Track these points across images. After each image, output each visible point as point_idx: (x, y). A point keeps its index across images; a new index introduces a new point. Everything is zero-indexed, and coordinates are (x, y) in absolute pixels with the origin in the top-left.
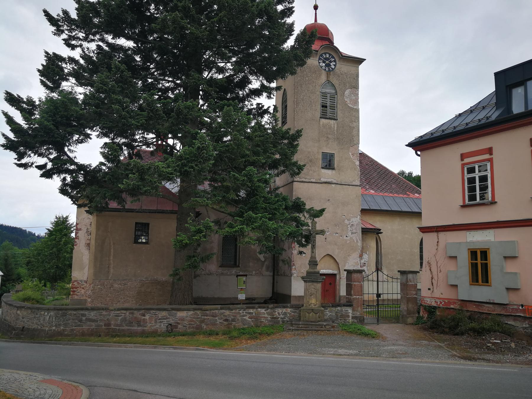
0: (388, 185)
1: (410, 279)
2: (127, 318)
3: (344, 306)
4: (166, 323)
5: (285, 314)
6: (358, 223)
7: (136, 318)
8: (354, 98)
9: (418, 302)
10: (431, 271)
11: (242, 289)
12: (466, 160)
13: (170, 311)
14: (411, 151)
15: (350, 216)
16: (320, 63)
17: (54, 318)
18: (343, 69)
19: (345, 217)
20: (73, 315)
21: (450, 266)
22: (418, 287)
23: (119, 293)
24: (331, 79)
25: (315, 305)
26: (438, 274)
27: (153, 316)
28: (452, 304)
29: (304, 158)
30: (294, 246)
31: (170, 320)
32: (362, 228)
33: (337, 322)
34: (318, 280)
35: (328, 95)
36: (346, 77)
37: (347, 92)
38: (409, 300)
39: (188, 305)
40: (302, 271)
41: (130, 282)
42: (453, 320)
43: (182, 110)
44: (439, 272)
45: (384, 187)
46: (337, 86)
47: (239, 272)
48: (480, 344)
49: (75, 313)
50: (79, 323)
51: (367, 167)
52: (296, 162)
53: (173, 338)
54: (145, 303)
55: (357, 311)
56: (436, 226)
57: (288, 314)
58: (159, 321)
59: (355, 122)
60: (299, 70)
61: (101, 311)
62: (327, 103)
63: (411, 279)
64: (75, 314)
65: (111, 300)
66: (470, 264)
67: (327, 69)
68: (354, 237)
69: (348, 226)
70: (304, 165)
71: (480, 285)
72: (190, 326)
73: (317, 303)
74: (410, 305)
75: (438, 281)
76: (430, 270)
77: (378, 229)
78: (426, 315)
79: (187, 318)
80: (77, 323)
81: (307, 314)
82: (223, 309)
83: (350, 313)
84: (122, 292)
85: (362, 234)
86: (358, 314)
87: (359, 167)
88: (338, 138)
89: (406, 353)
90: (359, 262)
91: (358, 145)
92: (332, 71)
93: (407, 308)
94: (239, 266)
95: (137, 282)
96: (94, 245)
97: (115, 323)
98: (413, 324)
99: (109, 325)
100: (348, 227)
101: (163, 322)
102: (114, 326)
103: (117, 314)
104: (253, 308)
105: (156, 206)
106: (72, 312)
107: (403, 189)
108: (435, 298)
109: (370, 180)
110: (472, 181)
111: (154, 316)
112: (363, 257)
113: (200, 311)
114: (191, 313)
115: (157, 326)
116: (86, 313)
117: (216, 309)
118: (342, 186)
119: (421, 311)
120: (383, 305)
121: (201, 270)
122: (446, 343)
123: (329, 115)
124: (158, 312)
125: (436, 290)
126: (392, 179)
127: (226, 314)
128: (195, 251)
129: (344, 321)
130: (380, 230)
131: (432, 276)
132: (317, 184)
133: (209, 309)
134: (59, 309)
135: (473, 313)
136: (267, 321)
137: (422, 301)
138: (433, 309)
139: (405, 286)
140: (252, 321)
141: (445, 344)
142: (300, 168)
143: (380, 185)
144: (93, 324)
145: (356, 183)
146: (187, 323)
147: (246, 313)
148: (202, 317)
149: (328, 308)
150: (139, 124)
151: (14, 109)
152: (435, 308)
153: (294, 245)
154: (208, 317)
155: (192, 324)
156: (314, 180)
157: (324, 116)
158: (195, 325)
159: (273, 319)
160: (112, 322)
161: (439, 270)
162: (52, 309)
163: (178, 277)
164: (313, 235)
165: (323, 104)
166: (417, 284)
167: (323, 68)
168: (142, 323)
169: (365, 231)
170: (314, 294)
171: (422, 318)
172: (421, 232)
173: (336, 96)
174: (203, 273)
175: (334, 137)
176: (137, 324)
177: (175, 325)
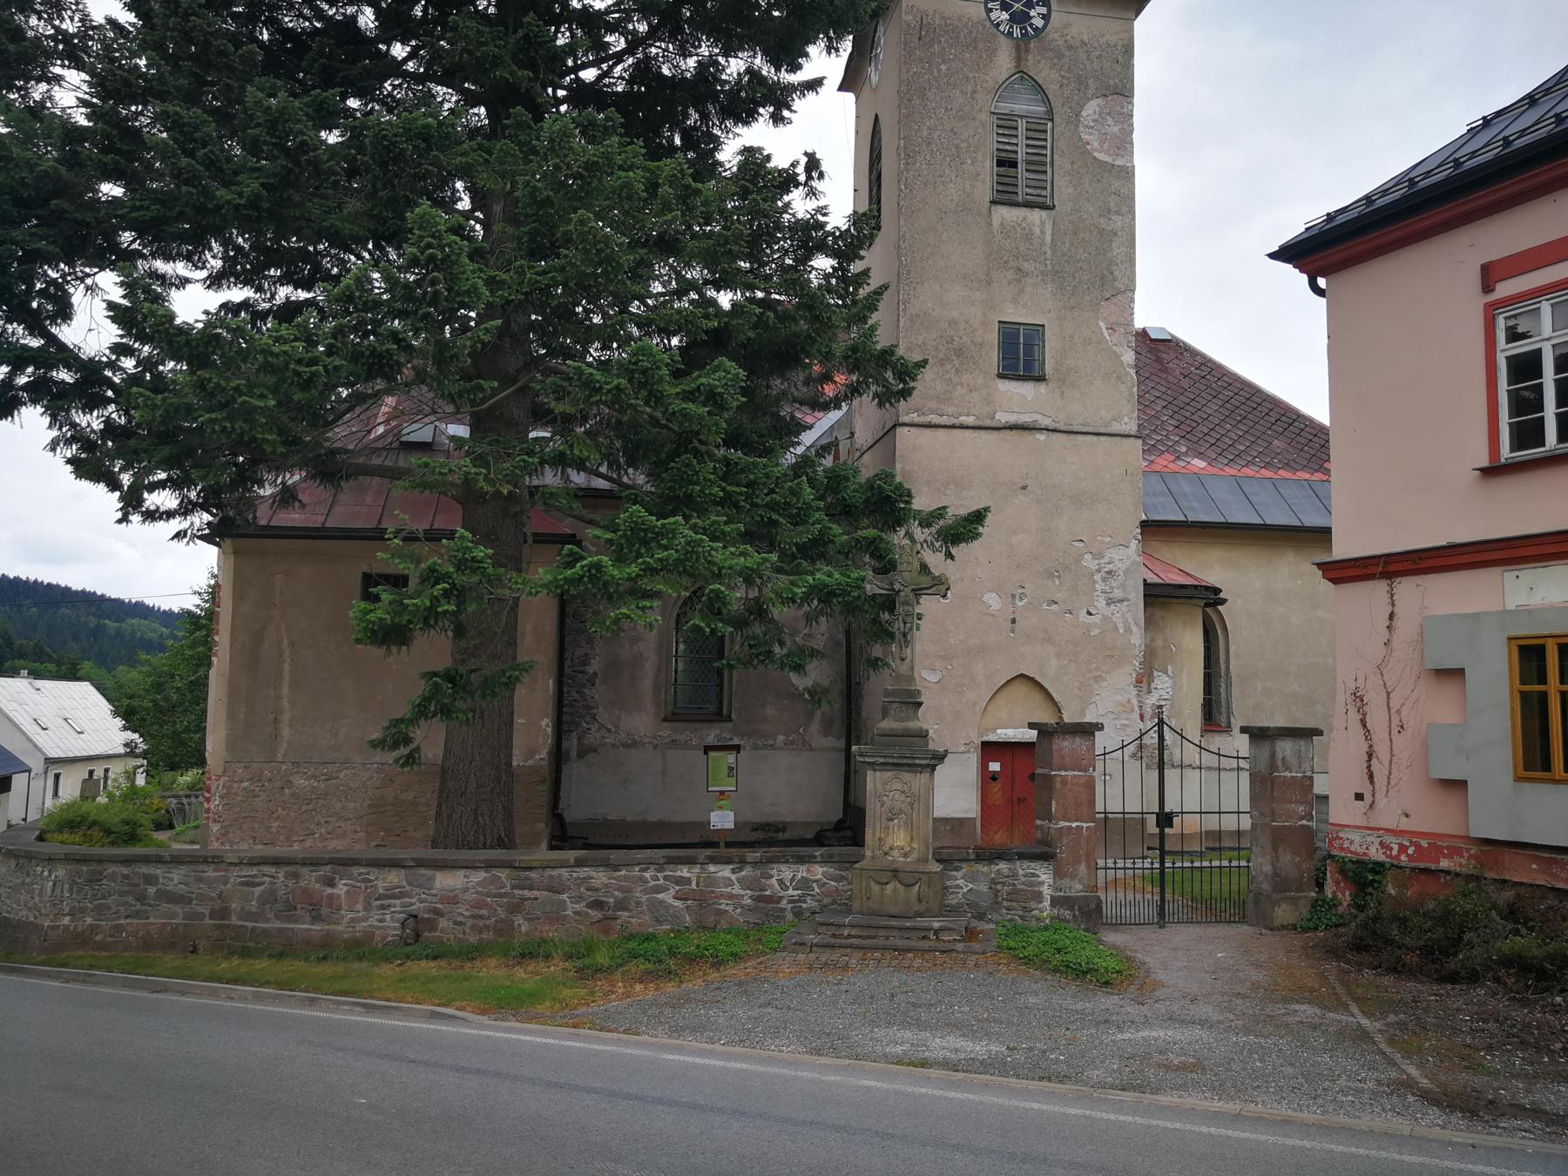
0: (1259, 441)
1: (1284, 758)
2: (281, 893)
3: (1022, 856)
4: (400, 913)
5: (805, 884)
7: (305, 891)
8: (1115, 129)
9: (1320, 844)
10: (1365, 726)
11: (722, 793)
12: (1504, 289)
13: (412, 871)
14: (1293, 278)
15: (1103, 542)
16: (991, 10)
17: (66, 886)
18: (1073, 31)
19: (1082, 544)
20: (119, 878)
21: (1440, 708)
22: (1318, 789)
23: (310, 807)
24: (1032, 64)
25: (906, 855)
26: (1391, 740)
27: (358, 884)
28: (1445, 857)
29: (934, 343)
31: (414, 900)
33: (996, 917)
34: (918, 762)
35: (1022, 125)
36: (1084, 56)
37: (1091, 109)
38: (1278, 838)
39: (492, 847)
41: (346, 768)
42: (1444, 918)
43: (393, 143)
44: (1395, 732)
45: (1242, 448)
46: (1051, 89)
47: (731, 739)
48: (1538, 1028)
49: (125, 871)
50: (139, 907)
51: (1185, 383)
52: (889, 352)
53: (401, 965)
54: (397, 838)
55: (1073, 877)
56: (1381, 556)
57: (815, 885)
58: (379, 903)
59: (1117, 213)
60: (916, 40)
61: (201, 867)
62: (1016, 152)
63: (1288, 759)
64: (126, 877)
65: (284, 827)
66: (1518, 696)
67: (1017, 32)
68: (1118, 614)
69: (1095, 577)
70: (924, 363)
71: (1559, 782)
72: (477, 922)
73: (915, 846)
74: (1287, 859)
75: (1390, 764)
76: (1363, 723)
77: (1207, 588)
78: (1347, 893)
79: (467, 896)
80: (132, 905)
81: (876, 888)
82: (586, 866)
83: (1043, 883)
84: (321, 801)
85: (1146, 605)
86: (1076, 888)
87: (1132, 372)
88: (1057, 272)
89: (1198, 1066)
90: (1135, 702)
91: (1129, 294)
92: (1033, 37)
93: (1273, 865)
94: (729, 719)
95: (369, 769)
96: (228, 648)
97: (242, 908)
98: (1295, 929)
99: (223, 913)
100: (1095, 582)
101: (389, 906)
102: (240, 919)
103: (249, 876)
104: (690, 861)
105: (431, 518)
106: (117, 870)
107: (1313, 452)
108: (1379, 829)
109: (1194, 425)
110: (1525, 367)
111: (363, 885)
112: (1153, 685)
113: (508, 871)
114: (478, 876)
115: (373, 922)
116: (158, 871)
117: (562, 864)
118: (1072, 436)
119: (1329, 880)
120: (1239, 849)
122: (1392, 1018)
123: (1022, 192)
124: (373, 874)
125: (1385, 800)
126: (1273, 420)
127: (595, 883)
128: (582, 668)
129: (1021, 913)
130: (1217, 591)
131: (1371, 746)
132: (982, 433)
133: (538, 864)
134: (77, 858)
135: (1523, 891)
136: (738, 911)
137: (1330, 841)
138: (1373, 871)
139: (1265, 784)
140: (687, 908)
141: (1387, 1025)
142: (907, 373)
143: (1227, 441)
144: (178, 909)
145: (1124, 426)
146: (466, 913)
147: (665, 878)
148: (516, 892)
150: (242, 202)
151: (213, 293)
152: (1378, 868)
154: (535, 892)
155: (481, 917)
156: (970, 420)
157: (1005, 196)
158: (493, 920)
159: (761, 905)
160: (234, 905)
161: (1395, 722)
162: (59, 857)
163: (404, 751)
164: (902, 594)
165: (1003, 154)
166: (1311, 778)
167: (1001, 28)
168: (324, 911)
169: (1158, 597)
170: (901, 812)
171: (1333, 904)
172: (1329, 580)
173: (1050, 124)
174: (607, 740)
175: (1043, 268)
176: (309, 911)
177: (428, 919)
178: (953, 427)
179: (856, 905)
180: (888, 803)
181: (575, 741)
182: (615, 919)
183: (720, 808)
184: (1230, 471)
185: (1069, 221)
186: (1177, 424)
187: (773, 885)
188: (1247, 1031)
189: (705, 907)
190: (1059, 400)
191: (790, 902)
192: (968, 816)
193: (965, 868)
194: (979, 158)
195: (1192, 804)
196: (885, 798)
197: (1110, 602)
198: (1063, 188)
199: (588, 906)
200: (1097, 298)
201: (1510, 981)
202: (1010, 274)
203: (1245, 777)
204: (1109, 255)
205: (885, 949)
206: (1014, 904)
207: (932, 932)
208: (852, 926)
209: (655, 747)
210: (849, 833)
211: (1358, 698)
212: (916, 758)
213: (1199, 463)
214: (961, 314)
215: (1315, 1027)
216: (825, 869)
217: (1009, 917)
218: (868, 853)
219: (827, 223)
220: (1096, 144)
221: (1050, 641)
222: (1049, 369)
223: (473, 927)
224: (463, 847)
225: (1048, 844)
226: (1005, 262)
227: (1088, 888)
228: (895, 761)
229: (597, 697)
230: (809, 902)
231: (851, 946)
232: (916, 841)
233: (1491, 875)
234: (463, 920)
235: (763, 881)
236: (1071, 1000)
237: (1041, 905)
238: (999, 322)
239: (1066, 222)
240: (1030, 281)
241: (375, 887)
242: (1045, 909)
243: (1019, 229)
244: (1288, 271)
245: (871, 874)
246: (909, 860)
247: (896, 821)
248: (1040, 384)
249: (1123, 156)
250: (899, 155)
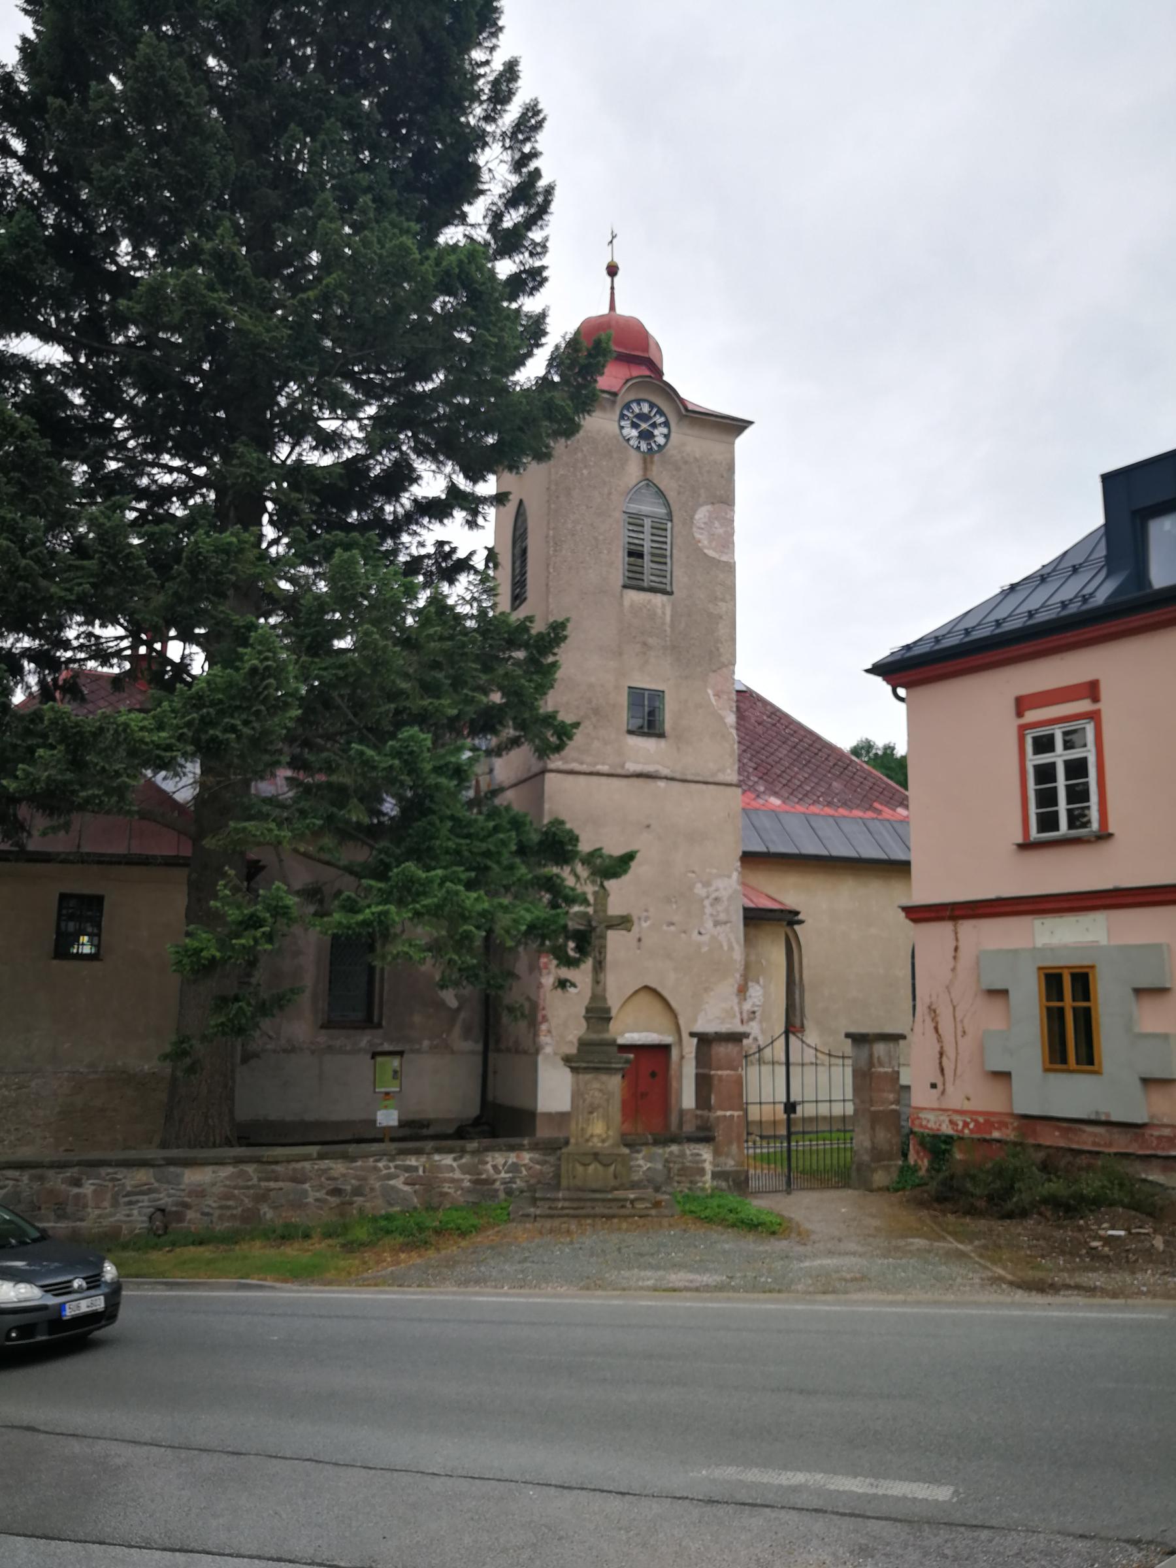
5: (515, 1168)
8: (721, 531)
9: (903, 1123)
11: (387, 1094)
12: (1032, 716)
14: (880, 685)
21: (991, 1018)
22: (904, 1081)
24: (656, 473)
25: (603, 1141)
27: (106, 1183)
31: (161, 1196)
33: (669, 1189)
35: (647, 523)
37: (702, 514)
38: (876, 1119)
42: (1000, 1172)
43: (205, 558)
44: (959, 1037)
45: (808, 788)
46: (671, 496)
47: (382, 1044)
51: (760, 729)
55: (728, 1155)
57: (523, 1169)
58: (127, 1199)
59: (723, 600)
70: (576, 725)
74: (882, 1136)
76: (936, 1029)
81: (580, 1169)
83: (705, 1161)
85: (746, 925)
86: (730, 1164)
87: (734, 732)
89: (863, 1278)
90: (736, 1009)
101: (138, 1202)
104: (418, 1152)
110: (1045, 774)
111: (110, 1184)
113: (255, 1166)
114: (226, 1171)
115: (120, 1216)
117: (306, 1158)
118: (686, 785)
122: (977, 1243)
123: (648, 579)
124: (121, 1173)
127: (334, 1173)
136: (459, 1192)
138: (945, 1142)
139: (865, 1079)
142: (565, 733)
146: (214, 1205)
147: (396, 1167)
148: (263, 1184)
149: (644, 1148)
152: (949, 1140)
155: (228, 1208)
156: (605, 768)
157: (634, 582)
158: (240, 1209)
159: (479, 1187)
163: (188, 1061)
166: (898, 1073)
167: (631, 442)
168: (70, 1209)
169: (755, 918)
170: (599, 1106)
171: (915, 1169)
173: (669, 524)
177: (176, 1212)
178: (591, 774)
182: (351, 1203)
184: (801, 808)
188: (885, 1257)
191: (502, 1183)
193: (645, 1151)
195: (810, 1095)
197: (716, 924)
198: (680, 577)
199: (327, 1194)
201: (1048, 1214)
203: (849, 1071)
208: (564, 1199)
209: (313, 1052)
210: (486, 1128)
211: (932, 1011)
213: (775, 801)
215: (929, 1252)
219: (530, 619)
220: (706, 543)
222: (668, 726)
223: (221, 1217)
224: (195, 1147)
227: (741, 1164)
231: (567, 1215)
233: (1031, 1141)
234: (211, 1211)
236: (751, 1244)
241: (123, 1185)
242: (708, 1181)
244: (878, 680)
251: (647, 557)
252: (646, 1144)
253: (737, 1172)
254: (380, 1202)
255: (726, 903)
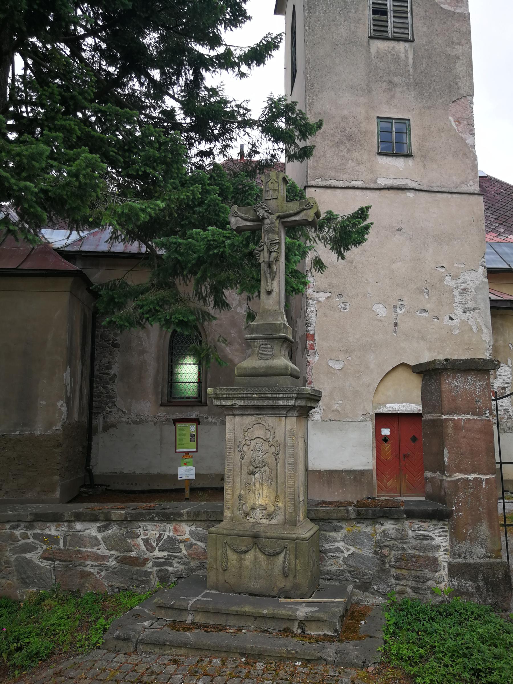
6: (481, 284)
11: (187, 453)
15: (458, 268)
19: (443, 270)
25: (270, 516)
29: (332, 132)
30: (312, 345)
32: (491, 301)
33: (383, 587)
34: (281, 403)
40: (336, 407)
47: (208, 418)
51: (499, 197)
55: (473, 540)
59: (459, 44)
62: (386, 5)
68: (472, 319)
73: (280, 505)
81: (233, 557)
83: (438, 547)
85: (493, 316)
88: (417, 84)
91: (470, 98)
94: (205, 405)
100: (454, 296)
109: (507, 218)
112: (498, 373)
118: (433, 194)
121: (120, 413)
123: (391, 31)
128: (106, 371)
129: (412, 584)
132: (368, 192)
136: (103, 573)
145: (470, 188)
147: (35, 536)
149: (344, 525)
153: (311, 342)
156: (360, 184)
159: (126, 567)
164: (267, 221)
165: (377, 6)
174: (123, 419)
175: (408, 81)
178: (347, 188)
179: (212, 577)
180: (249, 454)
181: (101, 420)
183: (185, 464)
185: (425, 49)
186: (496, 217)
187: (139, 546)
189: (71, 569)
190: (422, 170)
191: (156, 565)
192: (367, 468)
193: (346, 528)
194: (360, 9)
196: (245, 448)
197: (466, 311)
200: (446, 101)
202: (385, 85)
204: (454, 72)
205: (229, 650)
206: (404, 572)
207: (296, 624)
209: (155, 424)
212: (276, 394)
214: (350, 112)
216: (193, 528)
217: (398, 588)
218: (227, 513)
221: (423, 338)
222: (414, 149)
225: (442, 500)
226: (381, 77)
228: (255, 403)
229: (116, 390)
230: (175, 565)
232: (282, 498)
235: (129, 541)
237: (437, 575)
238: (378, 117)
239: (423, 50)
240: (398, 89)
243: (389, 55)
245: (228, 539)
246: (273, 522)
247: (257, 475)
248: (408, 159)
249: (461, 7)
250: (304, 9)
251: (390, 14)
252: (347, 519)
253: (491, 566)
254: (14, 580)
255: (474, 293)
